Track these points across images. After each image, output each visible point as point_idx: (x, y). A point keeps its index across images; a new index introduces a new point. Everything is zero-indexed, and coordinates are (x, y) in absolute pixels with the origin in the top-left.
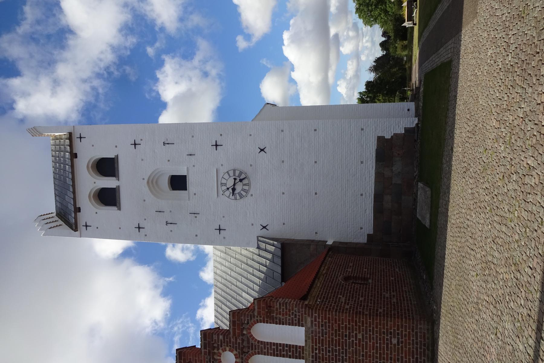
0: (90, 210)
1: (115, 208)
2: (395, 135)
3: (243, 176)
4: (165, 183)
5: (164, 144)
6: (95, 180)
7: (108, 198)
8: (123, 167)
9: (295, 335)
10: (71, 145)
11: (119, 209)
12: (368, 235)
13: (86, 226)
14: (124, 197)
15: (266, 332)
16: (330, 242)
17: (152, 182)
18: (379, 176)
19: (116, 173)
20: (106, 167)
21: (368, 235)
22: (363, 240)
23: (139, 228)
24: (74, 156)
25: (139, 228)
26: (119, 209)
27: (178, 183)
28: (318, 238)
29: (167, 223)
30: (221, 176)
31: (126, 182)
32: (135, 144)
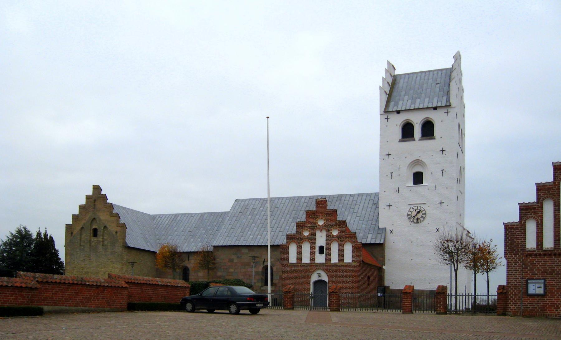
0: (398, 121)
1: (400, 137)
2: (406, 286)
3: (419, 221)
4: (418, 169)
5: (443, 170)
6: (419, 123)
7: (407, 131)
8: (428, 143)
9: (348, 259)
10: (441, 107)
11: (400, 141)
12: (389, 287)
13: (388, 118)
14: (408, 145)
15: (348, 249)
16: (384, 267)
17: (417, 162)
18: (422, 291)
19: (424, 138)
20: (428, 129)
21: (389, 287)
22: (386, 284)
23: (388, 155)
24: (435, 108)
25: (388, 155)
26: (400, 141)
27: (418, 178)
28: (386, 261)
29: (392, 173)
30: (422, 206)
31: (418, 147)
32: (442, 151)
